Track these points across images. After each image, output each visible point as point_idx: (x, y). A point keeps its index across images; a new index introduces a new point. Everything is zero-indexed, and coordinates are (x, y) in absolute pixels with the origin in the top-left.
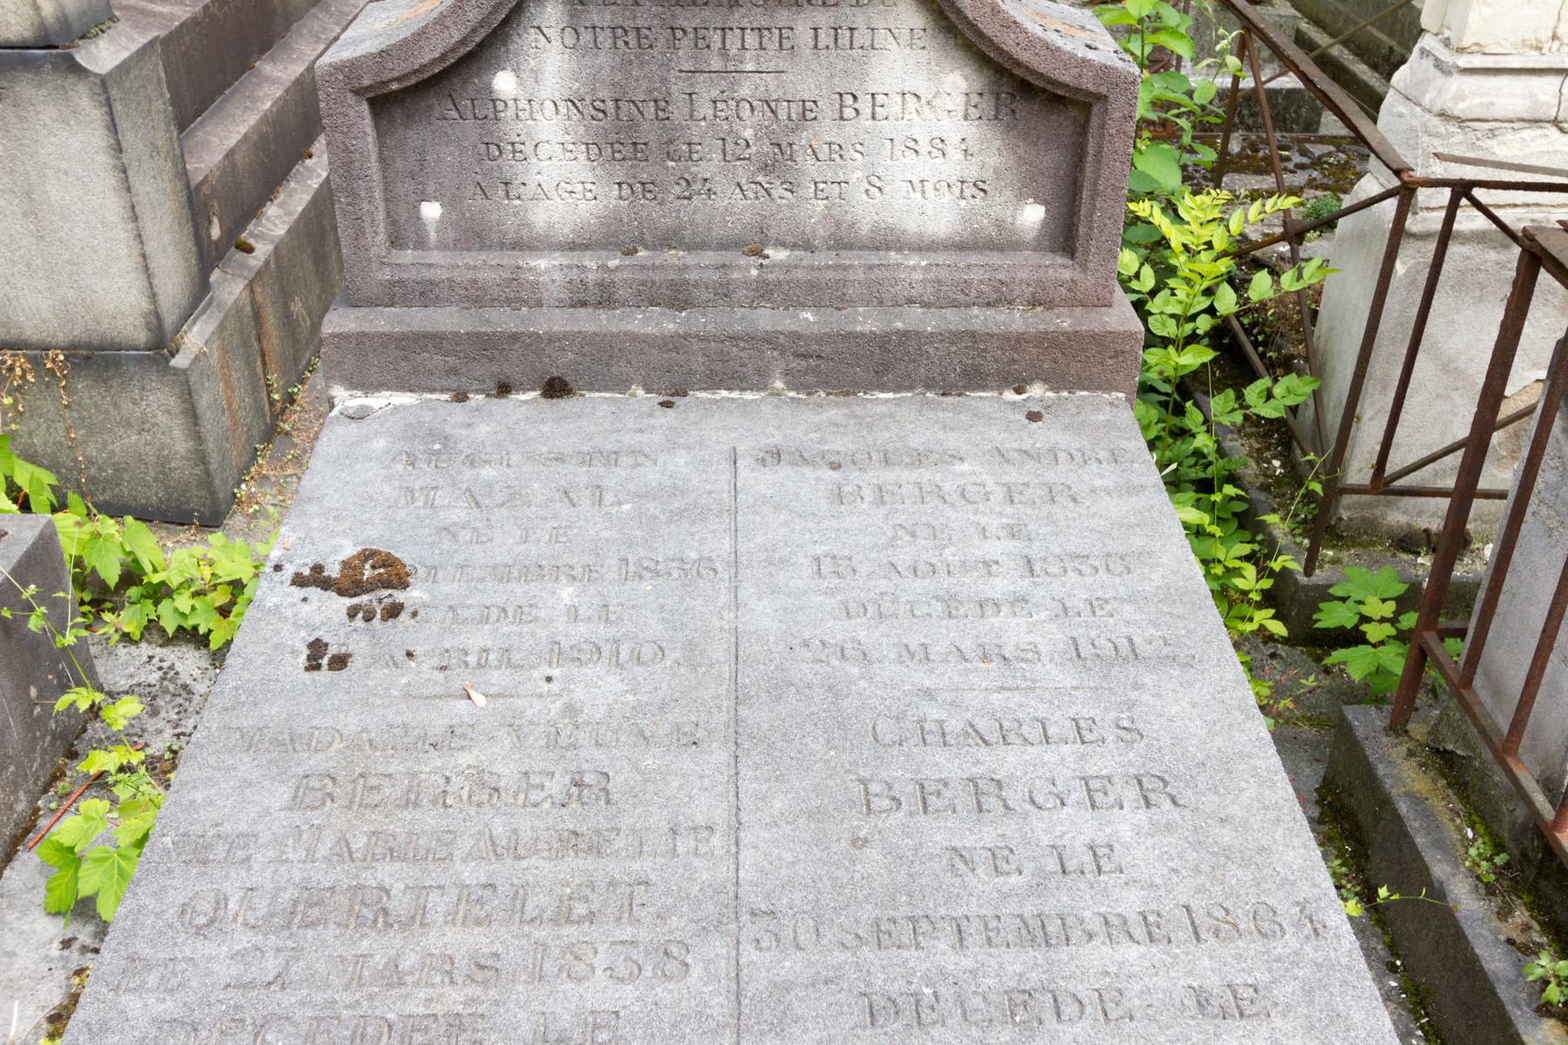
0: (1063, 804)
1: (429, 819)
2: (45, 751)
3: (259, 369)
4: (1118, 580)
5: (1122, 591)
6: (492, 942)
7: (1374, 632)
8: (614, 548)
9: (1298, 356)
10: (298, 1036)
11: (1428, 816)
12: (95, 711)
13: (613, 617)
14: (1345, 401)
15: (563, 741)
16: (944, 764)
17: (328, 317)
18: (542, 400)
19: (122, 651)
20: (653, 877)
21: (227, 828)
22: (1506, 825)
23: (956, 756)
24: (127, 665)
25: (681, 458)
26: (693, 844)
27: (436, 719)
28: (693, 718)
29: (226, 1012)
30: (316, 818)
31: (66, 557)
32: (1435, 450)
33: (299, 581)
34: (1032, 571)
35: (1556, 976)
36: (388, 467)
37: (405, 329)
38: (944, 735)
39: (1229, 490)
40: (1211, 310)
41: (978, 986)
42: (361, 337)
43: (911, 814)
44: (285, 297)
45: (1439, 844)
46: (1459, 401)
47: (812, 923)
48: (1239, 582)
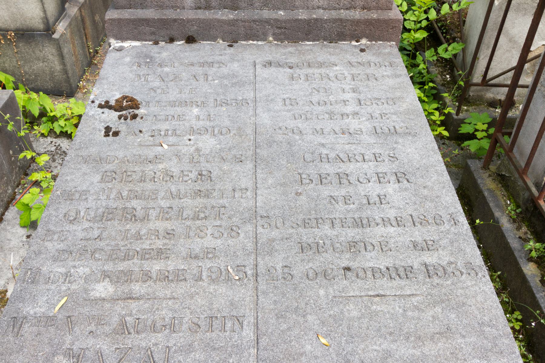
0: (369, 182)
1: (149, 186)
2: (16, 173)
3: (85, 40)
4: (391, 107)
5: (392, 111)
6: (172, 226)
7: (479, 135)
8: (212, 95)
9: (458, 37)
10: (106, 255)
11: (494, 196)
12: (33, 159)
13: (212, 119)
14: (473, 52)
15: (195, 160)
16: (328, 168)
17: (107, 13)
18: (185, 44)
19: (41, 140)
20: (227, 205)
21: (79, 189)
22: (521, 199)
23: (332, 166)
24: (43, 144)
25: (236, 65)
26: (241, 194)
27: (151, 153)
28: (240, 153)
29: (81, 248)
30: (110, 185)
31: (19, 105)
32: (505, 70)
33: (100, 106)
34: (360, 104)
35: (535, 249)
36: (131, 68)
37: (135, 17)
38: (328, 159)
39: (431, 84)
40: (427, 19)
41: (338, 240)
42: (119, 20)
43: (316, 185)
44: (93, 14)
45: (498, 206)
46: (514, 52)
47: (282, 220)
48: (433, 118)
